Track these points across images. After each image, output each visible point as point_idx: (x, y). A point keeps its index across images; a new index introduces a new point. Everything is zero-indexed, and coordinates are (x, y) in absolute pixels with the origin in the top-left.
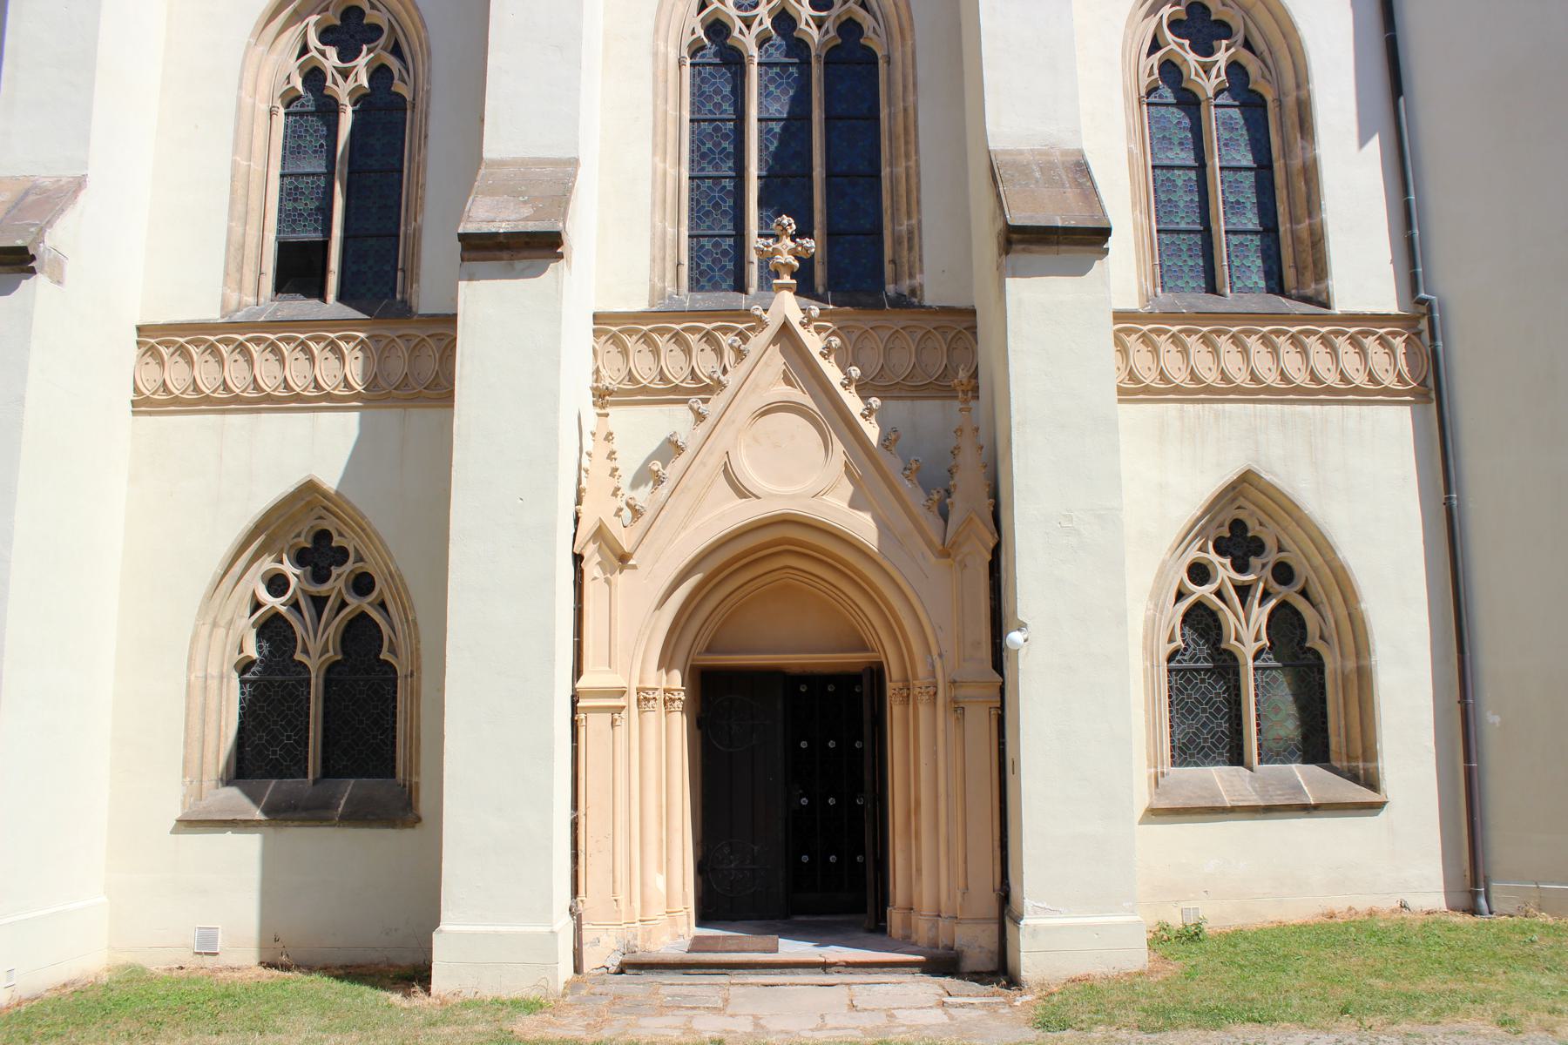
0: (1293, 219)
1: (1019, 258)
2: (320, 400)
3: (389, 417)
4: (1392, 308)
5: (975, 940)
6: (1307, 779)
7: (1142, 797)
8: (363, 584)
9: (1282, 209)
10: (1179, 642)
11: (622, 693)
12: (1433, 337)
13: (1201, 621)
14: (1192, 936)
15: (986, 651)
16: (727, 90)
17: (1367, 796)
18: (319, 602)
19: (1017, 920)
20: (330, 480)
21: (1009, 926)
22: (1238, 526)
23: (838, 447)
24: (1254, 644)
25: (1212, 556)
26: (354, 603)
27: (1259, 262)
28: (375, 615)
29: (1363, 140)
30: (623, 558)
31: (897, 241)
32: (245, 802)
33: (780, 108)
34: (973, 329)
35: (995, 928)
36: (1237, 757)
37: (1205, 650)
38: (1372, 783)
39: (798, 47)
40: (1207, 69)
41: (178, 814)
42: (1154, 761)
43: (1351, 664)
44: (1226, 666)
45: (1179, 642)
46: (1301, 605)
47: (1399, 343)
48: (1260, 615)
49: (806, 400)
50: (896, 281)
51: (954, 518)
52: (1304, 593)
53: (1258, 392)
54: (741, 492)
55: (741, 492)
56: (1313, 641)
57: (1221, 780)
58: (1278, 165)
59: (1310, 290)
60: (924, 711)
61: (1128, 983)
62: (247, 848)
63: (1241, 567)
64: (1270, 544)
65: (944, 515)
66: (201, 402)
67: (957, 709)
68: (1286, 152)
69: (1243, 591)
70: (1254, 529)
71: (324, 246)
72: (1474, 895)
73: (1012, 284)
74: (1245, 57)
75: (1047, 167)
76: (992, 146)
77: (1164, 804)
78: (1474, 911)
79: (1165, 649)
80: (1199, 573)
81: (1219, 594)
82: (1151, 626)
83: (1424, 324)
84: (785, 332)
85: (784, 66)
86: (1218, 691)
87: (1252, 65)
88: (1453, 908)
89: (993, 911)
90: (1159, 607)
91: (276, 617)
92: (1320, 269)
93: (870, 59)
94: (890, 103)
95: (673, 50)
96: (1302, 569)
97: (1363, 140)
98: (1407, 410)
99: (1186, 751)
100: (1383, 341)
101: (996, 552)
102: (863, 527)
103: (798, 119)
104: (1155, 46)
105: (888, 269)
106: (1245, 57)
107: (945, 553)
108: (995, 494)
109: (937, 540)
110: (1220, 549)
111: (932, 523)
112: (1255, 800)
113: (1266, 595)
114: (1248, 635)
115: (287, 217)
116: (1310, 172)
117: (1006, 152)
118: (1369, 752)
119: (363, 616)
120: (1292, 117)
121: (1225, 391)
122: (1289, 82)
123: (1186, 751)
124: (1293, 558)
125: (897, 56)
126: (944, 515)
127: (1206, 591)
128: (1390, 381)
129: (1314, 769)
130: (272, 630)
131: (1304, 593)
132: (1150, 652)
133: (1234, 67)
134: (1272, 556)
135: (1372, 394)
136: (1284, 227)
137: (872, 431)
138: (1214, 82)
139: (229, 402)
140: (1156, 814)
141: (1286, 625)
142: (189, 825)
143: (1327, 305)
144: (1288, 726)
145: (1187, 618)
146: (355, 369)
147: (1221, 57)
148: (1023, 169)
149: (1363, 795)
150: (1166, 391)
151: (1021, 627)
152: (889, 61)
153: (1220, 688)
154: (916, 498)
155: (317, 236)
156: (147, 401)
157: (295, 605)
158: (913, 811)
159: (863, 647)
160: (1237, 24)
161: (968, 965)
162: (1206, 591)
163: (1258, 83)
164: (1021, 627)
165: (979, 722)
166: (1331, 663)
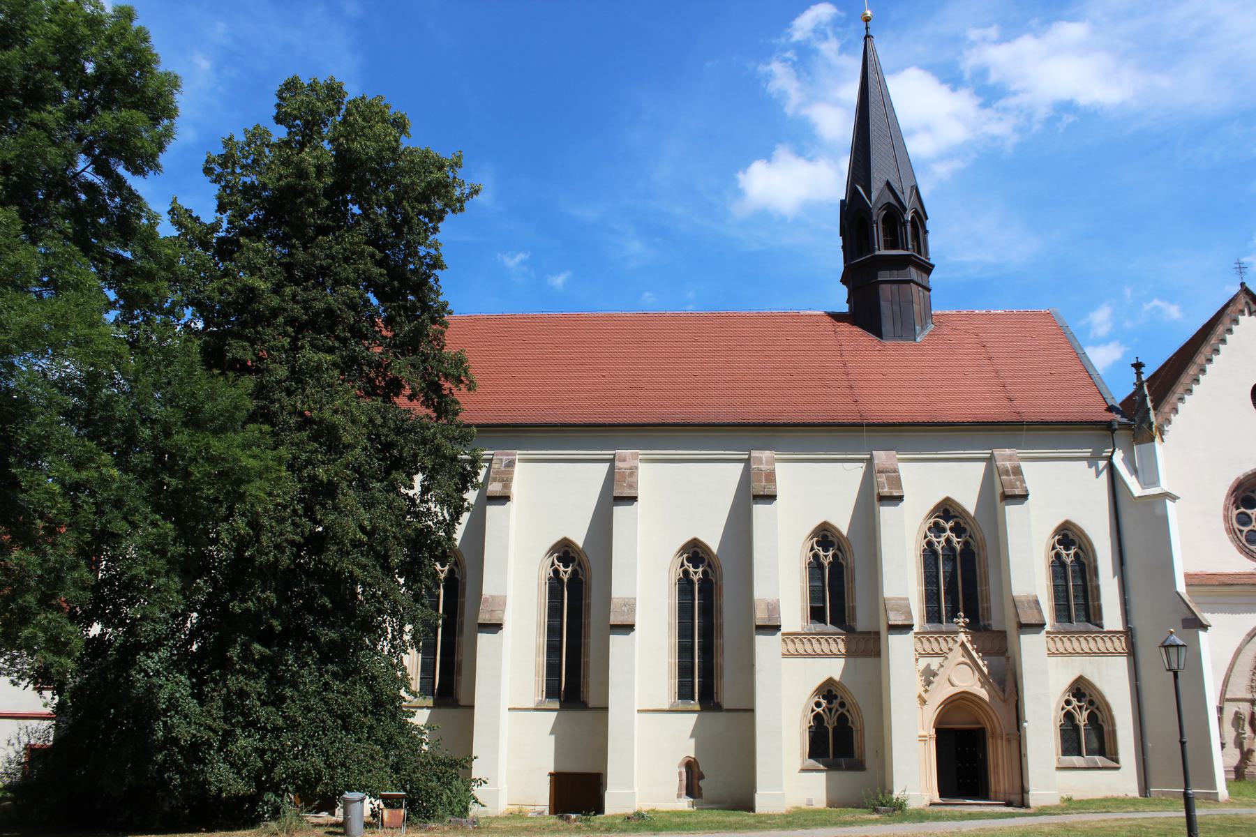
0: (1093, 601)
1: (1024, 630)
2: (833, 655)
3: (852, 660)
4: (1121, 629)
5: (1015, 798)
6: (1099, 760)
7: (1055, 764)
8: (842, 705)
9: (1090, 597)
10: (1063, 722)
11: (925, 737)
12: (1132, 638)
13: (1069, 716)
14: (1070, 800)
15: (1016, 726)
16: (933, 563)
17: (1116, 765)
18: (830, 710)
19: (1028, 793)
20: (837, 677)
21: (1025, 795)
22: (1078, 689)
23: (976, 673)
24: (885, 177)
25: (1071, 698)
26: (841, 710)
27: (1083, 613)
28: (847, 714)
29: (1114, 577)
30: (925, 702)
31: (983, 609)
32: (817, 764)
33: (949, 569)
34: (1006, 637)
35: (1020, 796)
36: (1080, 754)
37: (1070, 724)
38: (1117, 761)
39: (953, 549)
40: (1068, 555)
41: (800, 768)
42: (1057, 755)
43: (1111, 729)
44: (1076, 728)
45: (1063, 722)
46: (1096, 711)
47: (1123, 639)
48: (1085, 714)
49: (968, 661)
50: (983, 620)
51: (1007, 693)
52: (1097, 708)
53: (1084, 654)
54: (953, 685)
55: (953, 685)
56: (1100, 722)
57: (1076, 760)
58: (1089, 584)
59: (1098, 622)
60: (999, 741)
61: (1056, 807)
62: (822, 777)
63: (1079, 701)
64: (1087, 694)
65: (1004, 691)
66: (799, 655)
67: (1009, 741)
68: (1091, 580)
69: (1080, 708)
70: (1083, 690)
71: (824, 608)
72: (1146, 793)
73: (1022, 636)
74: (1080, 552)
75: (1029, 602)
76: (1014, 594)
77: (1060, 766)
78: (1146, 796)
79: (1059, 724)
80: (1068, 702)
81: (1073, 708)
82: (1055, 717)
83: (1130, 633)
84: (963, 645)
85: (949, 555)
86: (1074, 736)
87: (1081, 554)
88: (1140, 796)
89: (1020, 791)
90: (1057, 713)
91: (818, 713)
92: (1101, 618)
93: (973, 553)
94: (980, 568)
95: (919, 552)
96: (1097, 701)
97: (1114, 577)
98: (1125, 658)
99: (1066, 752)
100: (1118, 639)
101: (1017, 701)
102: (984, 694)
103: (954, 573)
104: (1053, 548)
105: (981, 618)
106: (1080, 552)
107: (1004, 701)
108: (1016, 686)
109: (1002, 697)
110: (1073, 696)
111: (1000, 693)
112: (1085, 766)
113: (1086, 709)
114: (1082, 720)
115: (812, 599)
116: (1097, 588)
117: (1018, 596)
118: (1116, 753)
119: (842, 714)
120: (1092, 570)
121: (1075, 654)
122: (1092, 560)
123: (1066, 752)
124: (1094, 698)
125: (981, 553)
126: (1004, 691)
127: (1069, 708)
128: (1120, 650)
129: (1102, 758)
130: (818, 717)
131: (1097, 708)
132: (1055, 725)
133: (1076, 554)
134: (1088, 698)
135: (1115, 654)
136: (1090, 603)
137: (985, 670)
138: (1071, 560)
139: (807, 655)
140: (1058, 769)
141: (1092, 718)
142: (803, 770)
143: (1102, 627)
144: (1095, 745)
145: (1065, 715)
146: (842, 647)
147: (1072, 552)
148: (1022, 603)
149: (1115, 765)
150: (1058, 654)
151: (1026, 722)
152: (979, 554)
153: (1074, 735)
154: (997, 687)
155: (821, 605)
156: (783, 654)
157: (823, 710)
158: (996, 766)
159: (979, 723)
160: (1076, 539)
161: (1014, 804)
162: (1069, 708)
163: (1082, 558)
164: (1026, 722)
165: (1014, 744)
166: (1106, 728)
